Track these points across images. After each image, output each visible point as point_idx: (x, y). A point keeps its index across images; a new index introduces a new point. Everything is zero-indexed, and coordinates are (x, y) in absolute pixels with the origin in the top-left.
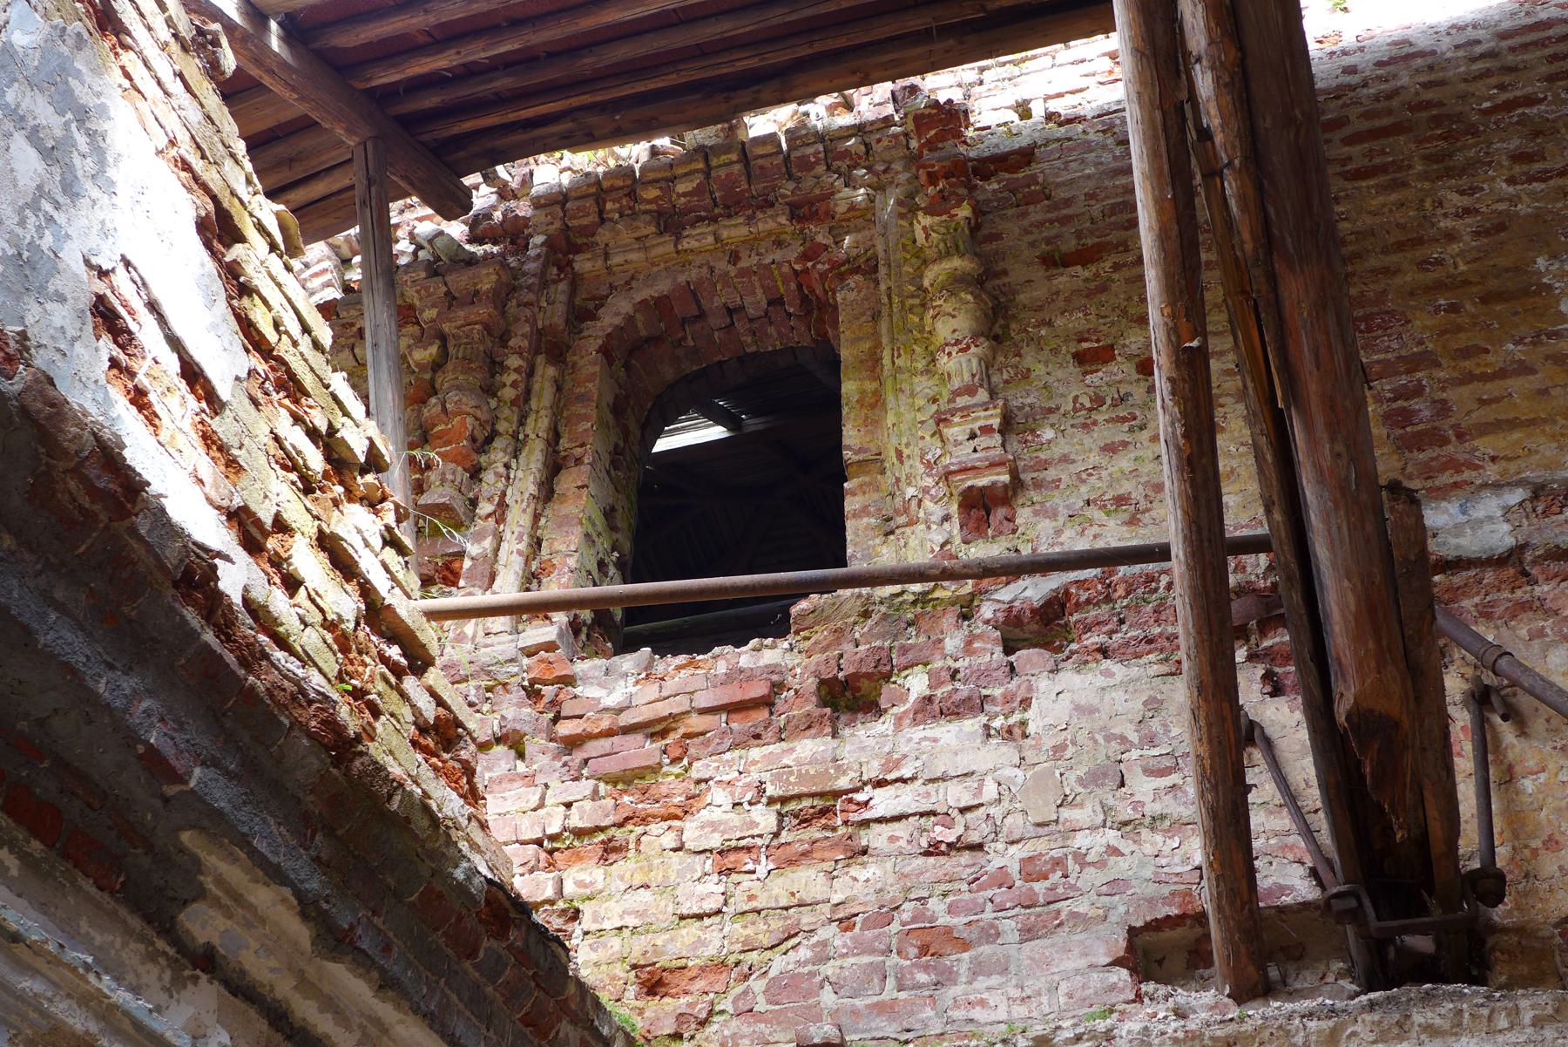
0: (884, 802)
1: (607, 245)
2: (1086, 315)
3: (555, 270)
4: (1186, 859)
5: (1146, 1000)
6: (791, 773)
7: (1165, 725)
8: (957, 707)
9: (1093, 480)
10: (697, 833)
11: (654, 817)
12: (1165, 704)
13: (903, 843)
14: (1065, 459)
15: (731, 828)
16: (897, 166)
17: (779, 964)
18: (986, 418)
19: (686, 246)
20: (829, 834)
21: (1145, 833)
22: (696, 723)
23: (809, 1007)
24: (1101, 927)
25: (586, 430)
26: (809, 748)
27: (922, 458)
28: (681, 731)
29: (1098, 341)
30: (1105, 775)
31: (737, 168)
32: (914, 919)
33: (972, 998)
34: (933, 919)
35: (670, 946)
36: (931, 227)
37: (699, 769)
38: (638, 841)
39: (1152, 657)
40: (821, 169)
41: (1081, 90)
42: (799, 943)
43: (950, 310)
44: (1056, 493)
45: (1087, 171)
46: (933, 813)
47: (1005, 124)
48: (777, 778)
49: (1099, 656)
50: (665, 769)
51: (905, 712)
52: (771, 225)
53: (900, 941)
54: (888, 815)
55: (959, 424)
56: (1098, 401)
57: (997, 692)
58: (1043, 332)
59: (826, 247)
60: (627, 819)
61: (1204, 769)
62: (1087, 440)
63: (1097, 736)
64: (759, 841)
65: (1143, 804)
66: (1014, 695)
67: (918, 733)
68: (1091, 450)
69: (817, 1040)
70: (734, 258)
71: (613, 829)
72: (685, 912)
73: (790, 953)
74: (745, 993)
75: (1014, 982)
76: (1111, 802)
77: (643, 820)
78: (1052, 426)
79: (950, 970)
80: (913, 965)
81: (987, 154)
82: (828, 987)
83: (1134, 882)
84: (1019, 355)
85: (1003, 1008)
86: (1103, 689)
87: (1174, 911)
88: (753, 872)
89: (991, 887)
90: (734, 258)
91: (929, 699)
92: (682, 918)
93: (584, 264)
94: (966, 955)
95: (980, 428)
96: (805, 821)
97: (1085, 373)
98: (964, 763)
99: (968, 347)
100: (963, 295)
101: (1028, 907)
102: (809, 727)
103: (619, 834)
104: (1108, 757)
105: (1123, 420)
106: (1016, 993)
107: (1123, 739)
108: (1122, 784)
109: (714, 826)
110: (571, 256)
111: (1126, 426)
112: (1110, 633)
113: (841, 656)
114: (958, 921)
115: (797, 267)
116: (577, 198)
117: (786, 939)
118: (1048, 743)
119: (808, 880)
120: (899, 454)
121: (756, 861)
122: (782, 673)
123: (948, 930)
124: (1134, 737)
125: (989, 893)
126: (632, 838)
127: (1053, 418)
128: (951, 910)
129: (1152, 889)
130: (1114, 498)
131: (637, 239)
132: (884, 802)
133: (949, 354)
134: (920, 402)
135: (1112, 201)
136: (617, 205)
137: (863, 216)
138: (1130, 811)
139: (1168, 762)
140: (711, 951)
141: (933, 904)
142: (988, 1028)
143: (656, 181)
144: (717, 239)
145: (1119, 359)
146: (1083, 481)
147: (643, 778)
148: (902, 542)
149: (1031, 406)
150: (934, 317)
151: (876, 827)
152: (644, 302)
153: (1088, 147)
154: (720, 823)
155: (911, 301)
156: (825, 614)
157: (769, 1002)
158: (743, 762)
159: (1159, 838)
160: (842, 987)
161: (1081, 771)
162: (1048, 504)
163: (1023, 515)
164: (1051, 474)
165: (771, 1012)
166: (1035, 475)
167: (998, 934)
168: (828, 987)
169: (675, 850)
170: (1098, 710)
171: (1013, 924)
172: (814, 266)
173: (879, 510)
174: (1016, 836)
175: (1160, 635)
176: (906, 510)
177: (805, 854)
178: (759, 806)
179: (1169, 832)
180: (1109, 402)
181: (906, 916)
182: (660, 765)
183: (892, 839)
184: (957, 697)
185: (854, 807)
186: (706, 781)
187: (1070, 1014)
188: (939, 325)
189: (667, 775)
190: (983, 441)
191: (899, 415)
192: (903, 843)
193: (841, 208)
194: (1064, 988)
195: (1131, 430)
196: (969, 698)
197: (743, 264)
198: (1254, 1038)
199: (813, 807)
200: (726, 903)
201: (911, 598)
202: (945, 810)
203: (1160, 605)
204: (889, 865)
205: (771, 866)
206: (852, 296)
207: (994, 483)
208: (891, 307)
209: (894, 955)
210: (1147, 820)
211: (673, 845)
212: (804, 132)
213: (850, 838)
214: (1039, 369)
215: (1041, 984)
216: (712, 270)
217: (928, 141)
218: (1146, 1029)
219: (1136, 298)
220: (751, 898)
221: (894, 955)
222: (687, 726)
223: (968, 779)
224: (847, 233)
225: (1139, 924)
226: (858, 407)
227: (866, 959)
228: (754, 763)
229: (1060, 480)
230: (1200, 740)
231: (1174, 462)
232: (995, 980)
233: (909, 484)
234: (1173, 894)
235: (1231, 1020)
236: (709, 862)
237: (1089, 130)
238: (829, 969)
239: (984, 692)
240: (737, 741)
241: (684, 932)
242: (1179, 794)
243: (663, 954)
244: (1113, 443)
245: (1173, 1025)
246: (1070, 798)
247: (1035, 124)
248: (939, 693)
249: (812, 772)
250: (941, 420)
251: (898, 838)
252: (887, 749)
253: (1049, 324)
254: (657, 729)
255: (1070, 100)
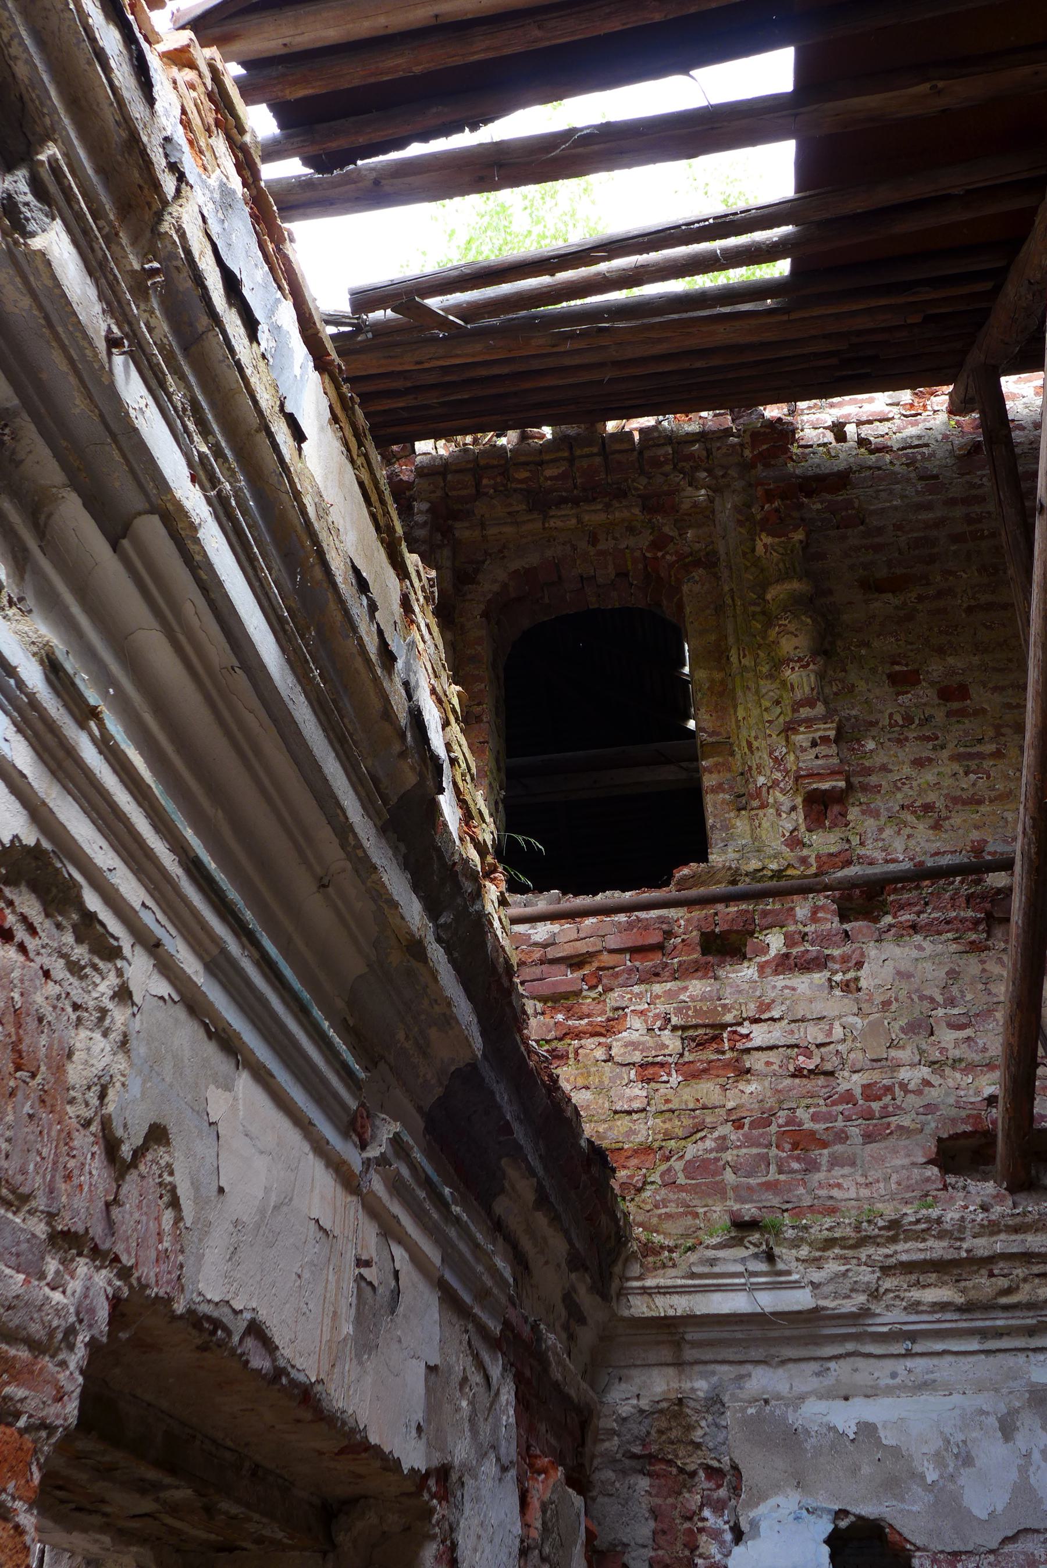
0: (759, 1035)
1: (483, 516)
2: (897, 640)
3: (439, 537)
4: (978, 1093)
5: (950, 1188)
6: (689, 1008)
7: (962, 992)
8: (808, 963)
9: (906, 788)
10: (622, 1051)
11: (585, 1033)
12: (962, 975)
13: (775, 1067)
14: (884, 768)
15: (648, 1048)
16: (733, 473)
17: (692, 1150)
18: (825, 730)
19: (552, 524)
20: (721, 1057)
21: (948, 1071)
22: (607, 959)
23: (716, 1183)
24: (919, 1137)
25: (481, 691)
26: (697, 987)
27: (771, 754)
28: (596, 964)
29: (907, 665)
30: (920, 1026)
31: (598, 460)
32: (787, 1124)
33: (831, 1182)
34: (800, 1124)
35: (609, 1133)
36: (772, 546)
37: (614, 998)
38: (577, 1054)
39: (950, 935)
40: (668, 468)
41: (888, 420)
42: (705, 1136)
43: (793, 630)
44: (878, 797)
45: (895, 503)
46: (797, 1046)
47: (825, 445)
48: (679, 1011)
49: (911, 932)
50: (584, 993)
51: (766, 962)
52: (626, 514)
53: (778, 1139)
54: (764, 1046)
55: (804, 733)
56: (908, 720)
57: (836, 952)
58: (863, 652)
59: (672, 538)
60: (566, 1034)
61: (1013, 1053)
62: (901, 754)
63: (913, 996)
64: (668, 1059)
65: (947, 1050)
66: (850, 957)
67: (780, 981)
68: (903, 763)
69: (747, 1218)
70: (594, 540)
71: (556, 1042)
72: (618, 1108)
73: (699, 1142)
74: (669, 1170)
75: (860, 1172)
76: (924, 1046)
77: (577, 1035)
78: (873, 738)
79: (815, 1161)
80: (789, 1156)
81: (810, 473)
82: (728, 1169)
83: (941, 1107)
84: (845, 671)
85: (853, 1190)
86: (917, 960)
87: (969, 1128)
88: (668, 1082)
89: (841, 1103)
90: (594, 540)
91: (787, 956)
92: (616, 1112)
93: (463, 531)
94: (825, 1151)
95: (820, 737)
96: (701, 1045)
97: (898, 694)
98: (819, 1008)
99: (808, 665)
100: (803, 618)
101: (868, 1119)
102: (696, 970)
103: (560, 1045)
104: (922, 1013)
105: (928, 739)
106: (861, 1180)
107: (932, 1000)
108: (932, 1034)
109: (634, 1045)
110: (450, 522)
111: (930, 745)
112: (918, 913)
113: (716, 914)
114: (819, 1127)
115: (648, 555)
116: (457, 472)
117: (695, 1133)
118: (878, 999)
119: (708, 1090)
120: (750, 745)
121: (669, 1074)
122: (669, 923)
123: (812, 1133)
124: (940, 999)
125: (840, 1108)
126: (571, 1049)
127: (874, 731)
128: (814, 1118)
129: (953, 1112)
130: (922, 806)
131: (509, 513)
132: (759, 1035)
133: (793, 669)
134: (766, 703)
135: (915, 535)
136: (492, 482)
137: (705, 515)
138: (937, 1054)
139: (964, 1020)
140: (640, 1138)
141: (799, 1113)
142: (843, 1203)
143: (527, 464)
144: (580, 521)
145: (924, 684)
146: (899, 789)
147: (567, 999)
148: (757, 822)
149: (856, 717)
150: (778, 633)
151: (757, 1055)
152: (516, 571)
153: (893, 478)
154: (640, 1043)
155: (753, 608)
156: (701, 880)
157: (687, 1177)
158: (649, 995)
159: (958, 1075)
160: (739, 1170)
161: (903, 1022)
162: (872, 806)
163: (853, 813)
164: (873, 780)
165: (690, 1185)
166: (861, 779)
167: (847, 1138)
168: (728, 1169)
169: (605, 1061)
170: (912, 976)
171: (858, 1131)
172: (663, 556)
173: (732, 788)
174: (858, 1067)
175: (956, 918)
176: (758, 795)
177: (705, 1071)
178: (667, 1032)
179: (966, 1071)
180: (917, 722)
181: (781, 1121)
182: (581, 991)
183: (768, 1064)
184: (809, 956)
185: (738, 1038)
186: (623, 1009)
187: (900, 1197)
188: (783, 641)
189: (586, 997)
190: (822, 750)
191: (746, 709)
192: (775, 1067)
193: (686, 506)
194: (894, 1177)
195: (934, 749)
196: (817, 958)
197: (601, 546)
198: (1032, 1226)
199: (706, 1034)
200: (648, 1104)
201: (770, 873)
202: (806, 1044)
203: (955, 894)
204: (767, 1083)
205: (680, 1079)
206: (697, 588)
207: (834, 788)
208: (735, 609)
209: (774, 1148)
210: (950, 1062)
211: (604, 1058)
212: (656, 434)
213: (737, 1061)
214: (862, 686)
215: (878, 1175)
216: (574, 548)
217: (760, 453)
218: (963, 1217)
219: (936, 629)
220: (667, 1101)
221: (774, 1148)
222: (599, 961)
223: (821, 1022)
224: (690, 527)
225: (945, 1136)
226: (709, 693)
227: (755, 1151)
228: (658, 997)
229: (880, 786)
230: (1013, 1035)
231: (1026, 867)
232: (847, 1170)
233: (760, 773)
234: (968, 1116)
235: (1018, 1214)
236: (633, 1072)
237: (895, 462)
238: (729, 1156)
239: (827, 952)
240: (642, 978)
241: (619, 1123)
242: (972, 1044)
243: (604, 1138)
244: (921, 758)
245: (981, 1216)
246: (895, 1042)
247: (850, 448)
248: (794, 951)
249: (705, 1008)
250: (789, 729)
251: (772, 1064)
252: (758, 993)
253: (867, 645)
254: (576, 962)
255: (883, 428)
